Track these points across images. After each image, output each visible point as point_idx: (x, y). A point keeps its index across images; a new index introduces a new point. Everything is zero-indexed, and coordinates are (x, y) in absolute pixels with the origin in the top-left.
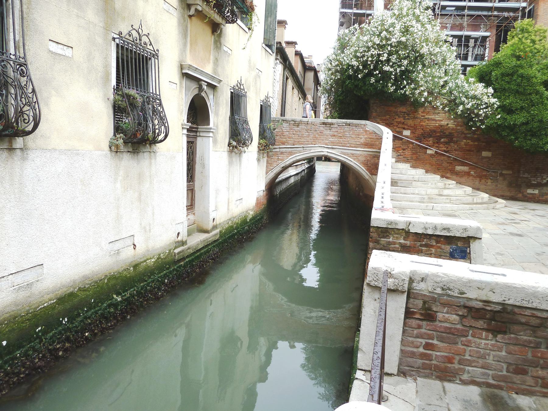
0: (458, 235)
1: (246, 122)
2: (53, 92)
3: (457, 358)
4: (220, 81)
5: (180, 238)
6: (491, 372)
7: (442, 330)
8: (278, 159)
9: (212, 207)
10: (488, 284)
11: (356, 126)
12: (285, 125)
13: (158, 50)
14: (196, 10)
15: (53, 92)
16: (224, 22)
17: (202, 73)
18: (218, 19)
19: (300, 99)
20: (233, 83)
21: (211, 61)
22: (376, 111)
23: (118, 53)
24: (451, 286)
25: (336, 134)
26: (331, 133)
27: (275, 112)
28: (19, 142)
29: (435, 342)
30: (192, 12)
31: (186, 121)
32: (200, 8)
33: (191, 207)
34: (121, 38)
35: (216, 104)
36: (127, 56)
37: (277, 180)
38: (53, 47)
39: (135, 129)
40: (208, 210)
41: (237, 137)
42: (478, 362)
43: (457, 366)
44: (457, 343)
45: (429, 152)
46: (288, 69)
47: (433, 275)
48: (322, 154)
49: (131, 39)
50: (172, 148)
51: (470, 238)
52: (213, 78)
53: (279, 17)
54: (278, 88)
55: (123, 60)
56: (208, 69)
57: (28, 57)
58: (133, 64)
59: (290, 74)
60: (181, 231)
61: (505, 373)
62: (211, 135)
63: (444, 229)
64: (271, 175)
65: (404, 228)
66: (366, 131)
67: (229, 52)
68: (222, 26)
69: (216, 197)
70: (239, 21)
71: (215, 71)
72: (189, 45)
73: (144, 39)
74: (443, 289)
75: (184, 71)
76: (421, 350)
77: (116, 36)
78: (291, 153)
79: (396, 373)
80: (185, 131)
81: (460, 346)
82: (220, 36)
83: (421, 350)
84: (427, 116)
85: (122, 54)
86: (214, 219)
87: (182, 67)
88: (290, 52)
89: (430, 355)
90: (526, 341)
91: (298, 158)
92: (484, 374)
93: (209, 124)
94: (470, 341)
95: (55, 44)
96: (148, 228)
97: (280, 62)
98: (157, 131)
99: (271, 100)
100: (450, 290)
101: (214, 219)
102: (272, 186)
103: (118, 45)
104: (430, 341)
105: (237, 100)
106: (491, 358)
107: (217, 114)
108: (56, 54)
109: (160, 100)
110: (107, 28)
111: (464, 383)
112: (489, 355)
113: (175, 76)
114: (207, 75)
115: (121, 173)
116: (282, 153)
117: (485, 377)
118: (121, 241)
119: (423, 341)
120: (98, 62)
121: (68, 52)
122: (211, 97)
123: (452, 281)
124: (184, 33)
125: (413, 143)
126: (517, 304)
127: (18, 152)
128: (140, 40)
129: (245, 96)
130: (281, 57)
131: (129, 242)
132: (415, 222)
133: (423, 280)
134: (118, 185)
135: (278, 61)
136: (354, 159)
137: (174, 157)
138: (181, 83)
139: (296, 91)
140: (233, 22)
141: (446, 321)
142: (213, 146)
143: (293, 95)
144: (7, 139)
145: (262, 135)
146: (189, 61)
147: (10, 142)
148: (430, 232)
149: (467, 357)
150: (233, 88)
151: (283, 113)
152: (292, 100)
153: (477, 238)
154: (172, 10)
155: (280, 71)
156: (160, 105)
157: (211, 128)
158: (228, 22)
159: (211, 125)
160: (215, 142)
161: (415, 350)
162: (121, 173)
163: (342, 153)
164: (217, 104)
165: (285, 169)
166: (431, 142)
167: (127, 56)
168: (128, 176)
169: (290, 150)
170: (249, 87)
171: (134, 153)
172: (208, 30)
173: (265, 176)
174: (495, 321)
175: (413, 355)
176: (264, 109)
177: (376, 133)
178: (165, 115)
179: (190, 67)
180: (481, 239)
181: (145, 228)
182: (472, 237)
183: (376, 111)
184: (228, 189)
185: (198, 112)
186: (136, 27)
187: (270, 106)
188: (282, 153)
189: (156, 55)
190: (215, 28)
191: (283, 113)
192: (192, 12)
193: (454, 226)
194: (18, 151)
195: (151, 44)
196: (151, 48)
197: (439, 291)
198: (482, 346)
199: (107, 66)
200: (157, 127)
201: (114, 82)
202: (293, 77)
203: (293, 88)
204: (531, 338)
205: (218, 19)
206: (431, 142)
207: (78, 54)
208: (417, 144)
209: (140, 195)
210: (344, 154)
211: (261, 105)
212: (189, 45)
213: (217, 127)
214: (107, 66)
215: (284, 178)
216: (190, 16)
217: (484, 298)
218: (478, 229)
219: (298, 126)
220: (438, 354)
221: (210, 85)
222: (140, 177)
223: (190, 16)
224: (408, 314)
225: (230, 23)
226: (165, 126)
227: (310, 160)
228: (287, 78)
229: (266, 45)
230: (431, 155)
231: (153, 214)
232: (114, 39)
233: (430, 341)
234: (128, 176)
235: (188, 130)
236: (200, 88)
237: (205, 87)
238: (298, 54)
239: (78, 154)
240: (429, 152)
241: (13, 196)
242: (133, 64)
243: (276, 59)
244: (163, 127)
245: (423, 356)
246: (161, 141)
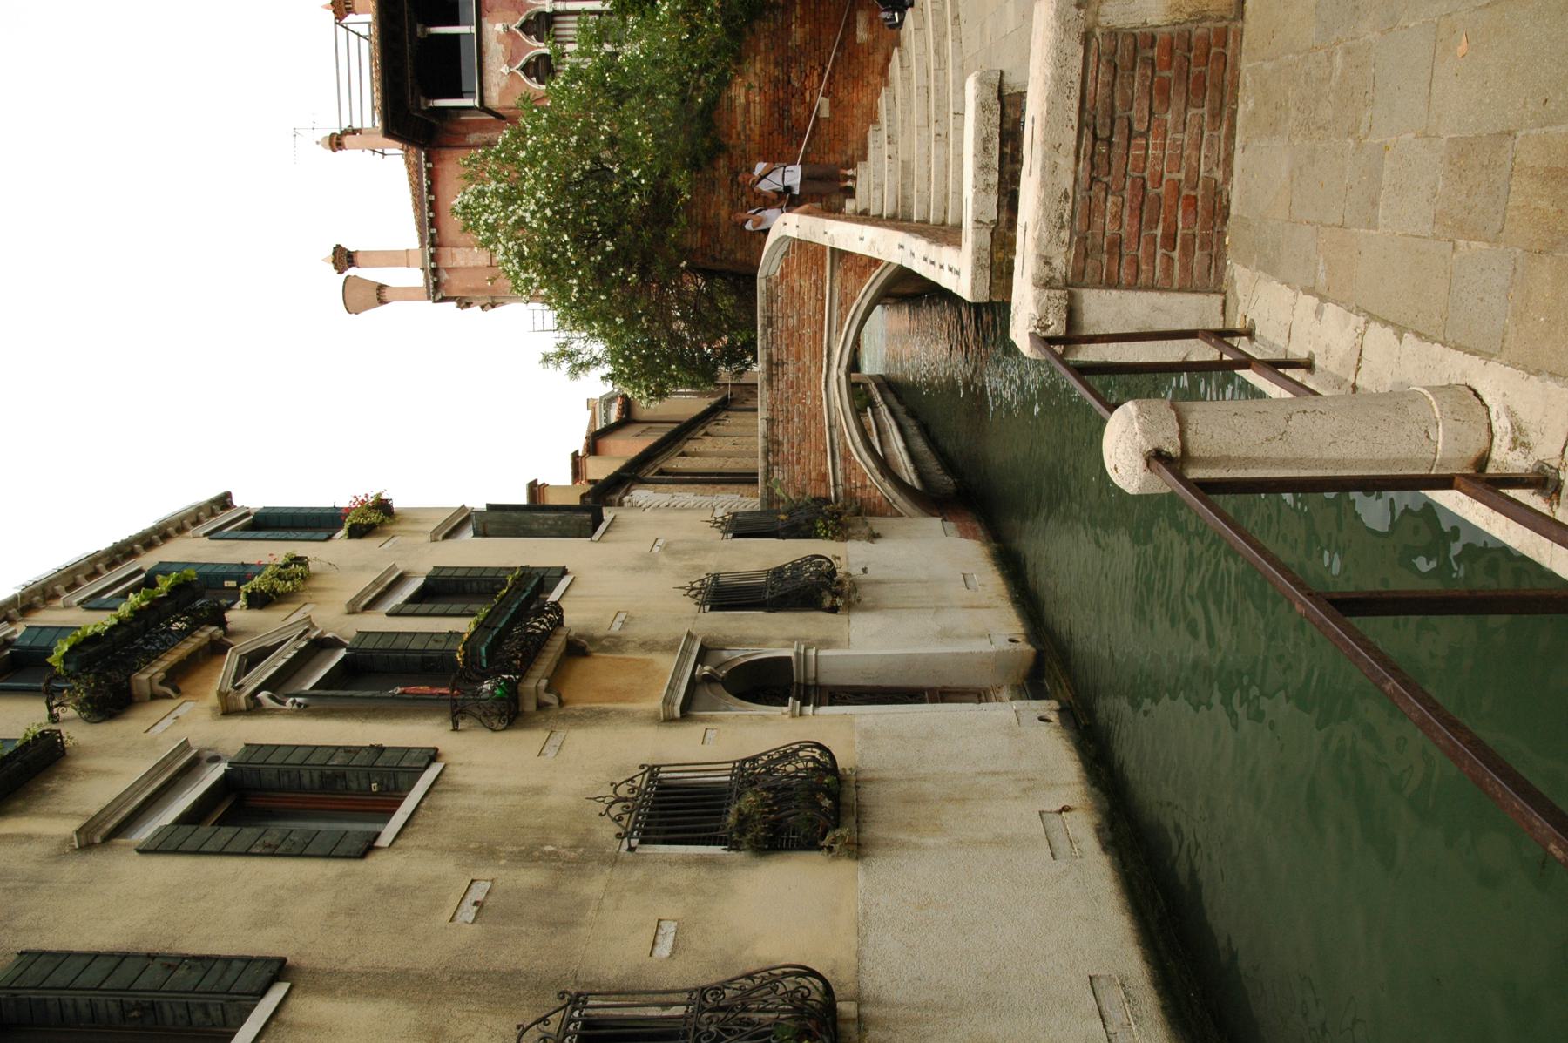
0: (996, 120)
1: (778, 572)
2: (747, 953)
3: (1185, 192)
4: (690, 636)
5: (1053, 717)
6: (1206, 134)
7: (1136, 222)
8: (864, 487)
9: (982, 646)
10: (1046, 156)
11: (771, 299)
12: (778, 475)
13: (642, 767)
14: (548, 690)
15: (747, 953)
16: (563, 632)
17: (676, 676)
18: (558, 643)
19: (706, 434)
20: (690, 606)
21: (649, 656)
22: (732, 252)
23: (655, 842)
24: (1054, 216)
25: (793, 349)
26: (792, 360)
27: (746, 501)
28: (846, 1008)
29: (1159, 232)
30: (550, 699)
31: (785, 709)
32: (544, 682)
33: (978, 695)
34: (628, 835)
35: (740, 645)
36: (660, 824)
37: (917, 485)
38: (664, 950)
39: (807, 812)
40: (988, 655)
41: (812, 591)
42: (1189, 157)
43: (1200, 192)
44: (1158, 196)
45: (825, 113)
46: (639, 470)
47: (1038, 247)
48: (843, 378)
49: (626, 817)
50: (846, 733)
51: (1001, 97)
52: (686, 652)
53: (522, 498)
54: (687, 496)
55: (668, 832)
56: (666, 663)
57: (689, 985)
58: (674, 812)
59: (651, 466)
60: (1036, 715)
61: (1205, 111)
62: (812, 652)
63: (985, 149)
64: (901, 503)
65: (988, 233)
66: (782, 275)
67: (622, 616)
68: (572, 634)
69: (959, 637)
70: (553, 597)
71: (670, 647)
72: (621, 706)
73: (623, 791)
74: (1062, 227)
75: (678, 714)
76: (1176, 254)
77: (625, 846)
78: (847, 457)
79: (1220, 298)
80: (809, 709)
81: (1162, 190)
82: (593, 640)
83: (1176, 254)
84: (739, 128)
85: (657, 832)
86: (1012, 641)
87: (669, 720)
88: (599, 469)
89: (1184, 236)
90: (1143, 85)
91: (857, 439)
92: (1210, 145)
93: (789, 658)
94: (1152, 175)
95: (657, 949)
96: (1026, 784)
97: (626, 493)
98: (810, 765)
99: (719, 513)
100: (1061, 216)
101: (1012, 641)
102: (930, 501)
103: (642, 842)
104: (1159, 240)
105: (725, 595)
106: (1179, 136)
107: (763, 641)
108: (675, 947)
109: (744, 761)
110: (615, 861)
111: (1228, 173)
112: (1175, 140)
113: (693, 732)
114: (680, 666)
115: (902, 836)
116: (847, 479)
117: (1216, 142)
118: (1053, 836)
119: (1160, 252)
120: (682, 877)
121: (669, 928)
122: (726, 655)
123: (1047, 216)
124: (597, 717)
125: (805, 153)
126: (1076, 105)
127: (866, 1010)
128: (626, 800)
129: (716, 577)
130: (615, 492)
131: (1055, 821)
132: (974, 211)
133: (1047, 263)
134: (930, 841)
135: (626, 498)
136: (854, 299)
137: (867, 731)
138: (703, 720)
139: (690, 446)
140: (557, 608)
141: (1118, 217)
142: (838, 647)
143: (707, 452)
144: (841, 1026)
145: (808, 533)
146: (655, 704)
147: (847, 1021)
148: (994, 178)
149: (1182, 176)
150: (703, 604)
151: (745, 479)
152: (712, 455)
153: (1001, 81)
154: (556, 739)
155: (646, 492)
156: (754, 759)
157: (798, 654)
158: (560, 622)
159: (789, 653)
160: (827, 643)
161: (1177, 265)
162: (902, 836)
163: (839, 330)
164: (739, 642)
165: (885, 466)
166: (801, 110)
167: (660, 824)
168: (910, 824)
169: (838, 460)
170: (694, 568)
171: (859, 813)
172: (582, 665)
173: (906, 519)
174: (1111, 136)
175: (1187, 269)
176: (741, 528)
177: (787, 253)
178: (776, 750)
179: (667, 701)
180: (1002, 73)
181: (1024, 790)
182: (1000, 91)
183: (732, 252)
184: (938, 609)
185: (767, 683)
186: (602, 807)
187: (735, 515)
188: (847, 479)
189: (652, 771)
190: (577, 649)
191: (745, 479)
192: (550, 699)
193: (978, 131)
194: (862, 1010)
195: (632, 780)
196: (638, 780)
197: (1065, 234)
198: (1158, 152)
199: (687, 862)
200: (801, 765)
201: (716, 850)
202: (656, 457)
203: (683, 454)
204: (1137, 74)
205: (558, 643)
206: (801, 110)
207: (671, 910)
208: (808, 144)
209: (950, 800)
210: (842, 325)
211: (735, 536)
212: (621, 706)
213: (792, 640)
214: (687, 862)
215: (910, 468)
216: (561, 703)
217: (1072, 158)
218: (981, 81)
219: (779, 443)
220: (1180, 225)
221: (701, 659)
222: (910, 800)
223: (561, 703)
224: (1112, 284)
225: (562, 617)
226: (801, 749)
227: (859, 396)
228: (661, 472)
229: (595, 530)
230: (834, 106)
231: (994, 773)
232: (631, 849)
233: (1159, 240)
234: (910, 824)
235: (805, 703)
236: (709, 679)
237: (707, 668)
238: (595, 443)
239: (866, 914)
240: (825, 113)
241: (950, 1020)
242: (674, 812)
243: (621, 504)
244: (801, 754)
245: (1187, 253)
246: (832, 757)
